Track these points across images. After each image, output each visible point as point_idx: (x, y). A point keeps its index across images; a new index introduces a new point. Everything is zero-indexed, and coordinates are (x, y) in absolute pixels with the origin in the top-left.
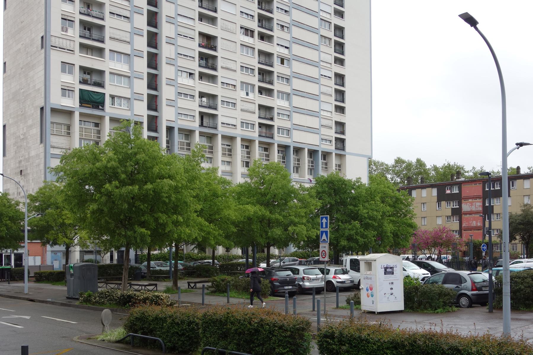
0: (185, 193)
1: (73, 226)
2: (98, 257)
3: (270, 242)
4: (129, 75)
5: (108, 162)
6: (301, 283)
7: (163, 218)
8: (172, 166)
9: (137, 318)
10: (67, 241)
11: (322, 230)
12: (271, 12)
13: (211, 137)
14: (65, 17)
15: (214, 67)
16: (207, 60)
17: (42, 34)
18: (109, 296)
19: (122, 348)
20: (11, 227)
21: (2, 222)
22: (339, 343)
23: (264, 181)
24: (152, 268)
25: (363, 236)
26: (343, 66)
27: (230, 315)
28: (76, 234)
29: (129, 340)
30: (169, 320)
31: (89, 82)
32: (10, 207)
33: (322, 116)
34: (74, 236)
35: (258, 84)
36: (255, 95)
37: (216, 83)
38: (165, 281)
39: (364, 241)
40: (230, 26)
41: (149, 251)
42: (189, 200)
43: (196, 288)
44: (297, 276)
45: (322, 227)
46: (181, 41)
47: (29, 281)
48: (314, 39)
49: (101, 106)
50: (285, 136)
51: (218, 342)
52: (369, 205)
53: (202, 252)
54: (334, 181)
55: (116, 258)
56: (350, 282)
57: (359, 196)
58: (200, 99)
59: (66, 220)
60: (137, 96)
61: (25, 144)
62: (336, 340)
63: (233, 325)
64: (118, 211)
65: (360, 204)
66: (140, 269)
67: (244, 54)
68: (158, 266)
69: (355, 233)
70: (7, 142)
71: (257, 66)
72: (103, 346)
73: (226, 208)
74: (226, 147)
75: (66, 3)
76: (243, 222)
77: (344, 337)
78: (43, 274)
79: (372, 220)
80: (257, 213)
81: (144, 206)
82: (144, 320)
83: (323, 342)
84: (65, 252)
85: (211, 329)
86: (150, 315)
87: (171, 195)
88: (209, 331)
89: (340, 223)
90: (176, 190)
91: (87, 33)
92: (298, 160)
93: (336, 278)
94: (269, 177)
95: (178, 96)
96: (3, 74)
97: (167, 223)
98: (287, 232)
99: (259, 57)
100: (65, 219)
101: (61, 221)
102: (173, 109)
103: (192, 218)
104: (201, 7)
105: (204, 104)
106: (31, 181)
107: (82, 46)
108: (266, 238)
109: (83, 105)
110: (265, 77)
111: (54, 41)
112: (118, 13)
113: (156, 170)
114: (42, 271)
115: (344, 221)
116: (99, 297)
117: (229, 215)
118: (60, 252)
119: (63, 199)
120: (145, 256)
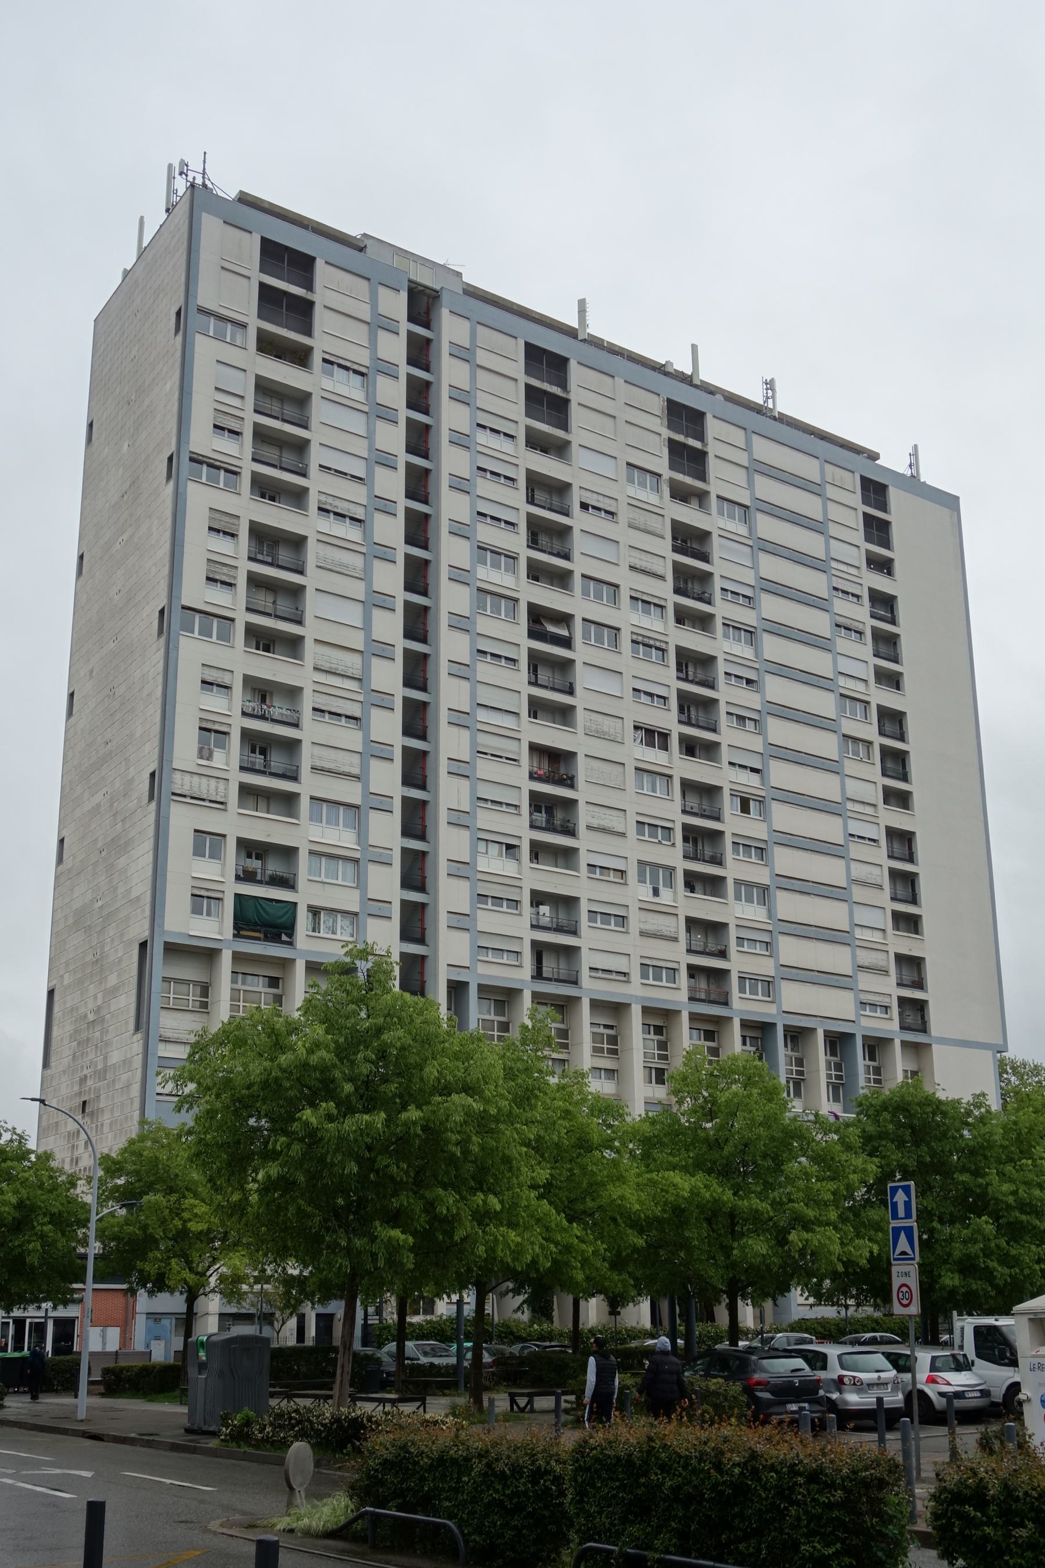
0: (508, 1132)
1: (206, 1237)
2: (267, 1332)
3: (737, 1277)
4: (357, 855)
5: (310, 1051)
6: (834, 1396)
7: (448, 1200)
8: (472, 1062)
9: (386, 1461)
10: (191, 1278)
11: (894, 1223)
12: (711, 685)
13: (563, 1006)
14: (209, 726)
15: (567, 827)
16: (550, 811)
17: (153, 766)
18: (299, 1422)
19: (343, 1552)
20: (55, 1241)
21: (34, 1228)
22: (1004, 1519)
23: (715, 1108)
24: (408, 1359)
25: (1006, 1260)
26: (908, 809)
27: (657, 1444)
28: (215, 1260)
29: (362, 1529)
30: (478, 1467)
31: (259, 878)
32: (55, 1188)
33: (858, 943)
34: (209, 1267)
35: (682, 865)
36: (675, 893)
37: (576, 868)
38: (444, 1395)
39: (1010, 1275)
40: (608, 725)
41: (402, 1313)
42: (517, 1151)
43: (532, 1411)
44: (821, 1375)
45: (895, 1216)
46: (485, 768)
47: (90, 1393)
48: (826, 745)
49: (285, 934)
50: (760, 997)
51: (621, 1527)
52: (1017, 1171)
53: (544, 1319)
54: (909, 1103)
55: (313, 1333)
56: (979, 1394)
57: (985, 1144)
58: (534, 910)
59: (191, 1223)
60: (374, 908)
61: (98, 1034)
62: (992, 1509)
63: (668, 1474)
64: (332, 1182)
65: (989, 1168)
66: (378, 1361)
67: (645, 792)
68: (426, 1354)
69: (981, 1249)
70: (56, 1032)
71: (679, 820)
72: (289, 1544)
73: (612, 1181)
74: (602, 1030)
75: (212, 691)
76: (659, 1220)
77: (1018, 1499)
78: (124, 1372)
79: (1029, 1214)
80: (698, 1194)
81: (398, 1167)
82: (407, 1468)
83: (951, 1518)
84: (185, 1317)
85: (600, 1488)
86: (423, 1452)
87: (469, 1137)
88: (594, 1496)
89: (936, 1224)
90: (483, 1123)
91: (257, 760)
92: (800, 1062)
93: (937, 1383)
94: (727, 1094)
95: (478, 903)
96: (57, 867)
97: (458, 1214)
98: (786, 1248)
99: (684, 798)
100: (190, 1220)
101: (179, 1224)
102: (466, 936)
103: (524, 1203)
104: (534, 683)
105: (545, 921)
106: (106, 1129)
107: (247, 792)
108: (727, 1267)
109: (242, 933)
110: (700, 847)
111: (179, 782)
112: (333, 710)
113: (431, 1071)
114: (122, 1363)
115: (947, 1217)
116: (271, 1424)
117: (622, 1198)
118: (170, 1316)
119: (193, 1151)
120: (388, 1327)
